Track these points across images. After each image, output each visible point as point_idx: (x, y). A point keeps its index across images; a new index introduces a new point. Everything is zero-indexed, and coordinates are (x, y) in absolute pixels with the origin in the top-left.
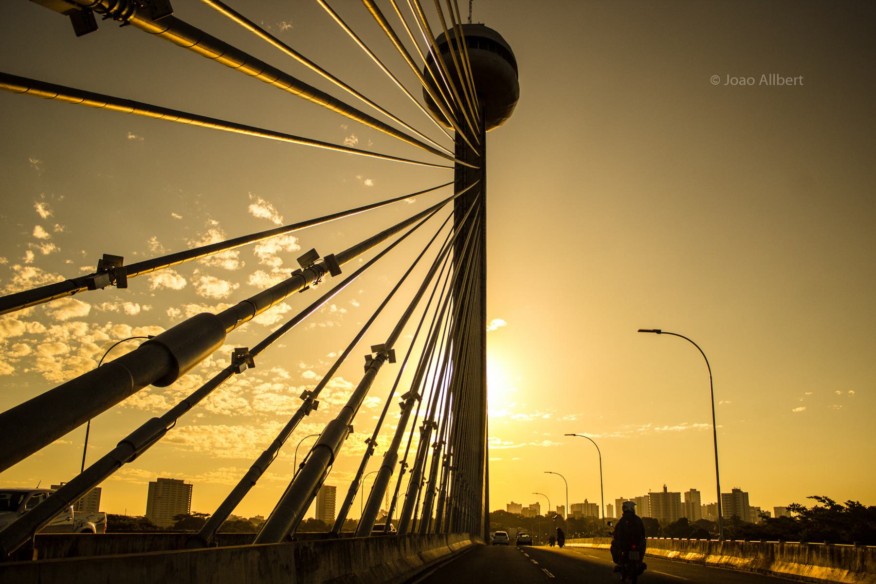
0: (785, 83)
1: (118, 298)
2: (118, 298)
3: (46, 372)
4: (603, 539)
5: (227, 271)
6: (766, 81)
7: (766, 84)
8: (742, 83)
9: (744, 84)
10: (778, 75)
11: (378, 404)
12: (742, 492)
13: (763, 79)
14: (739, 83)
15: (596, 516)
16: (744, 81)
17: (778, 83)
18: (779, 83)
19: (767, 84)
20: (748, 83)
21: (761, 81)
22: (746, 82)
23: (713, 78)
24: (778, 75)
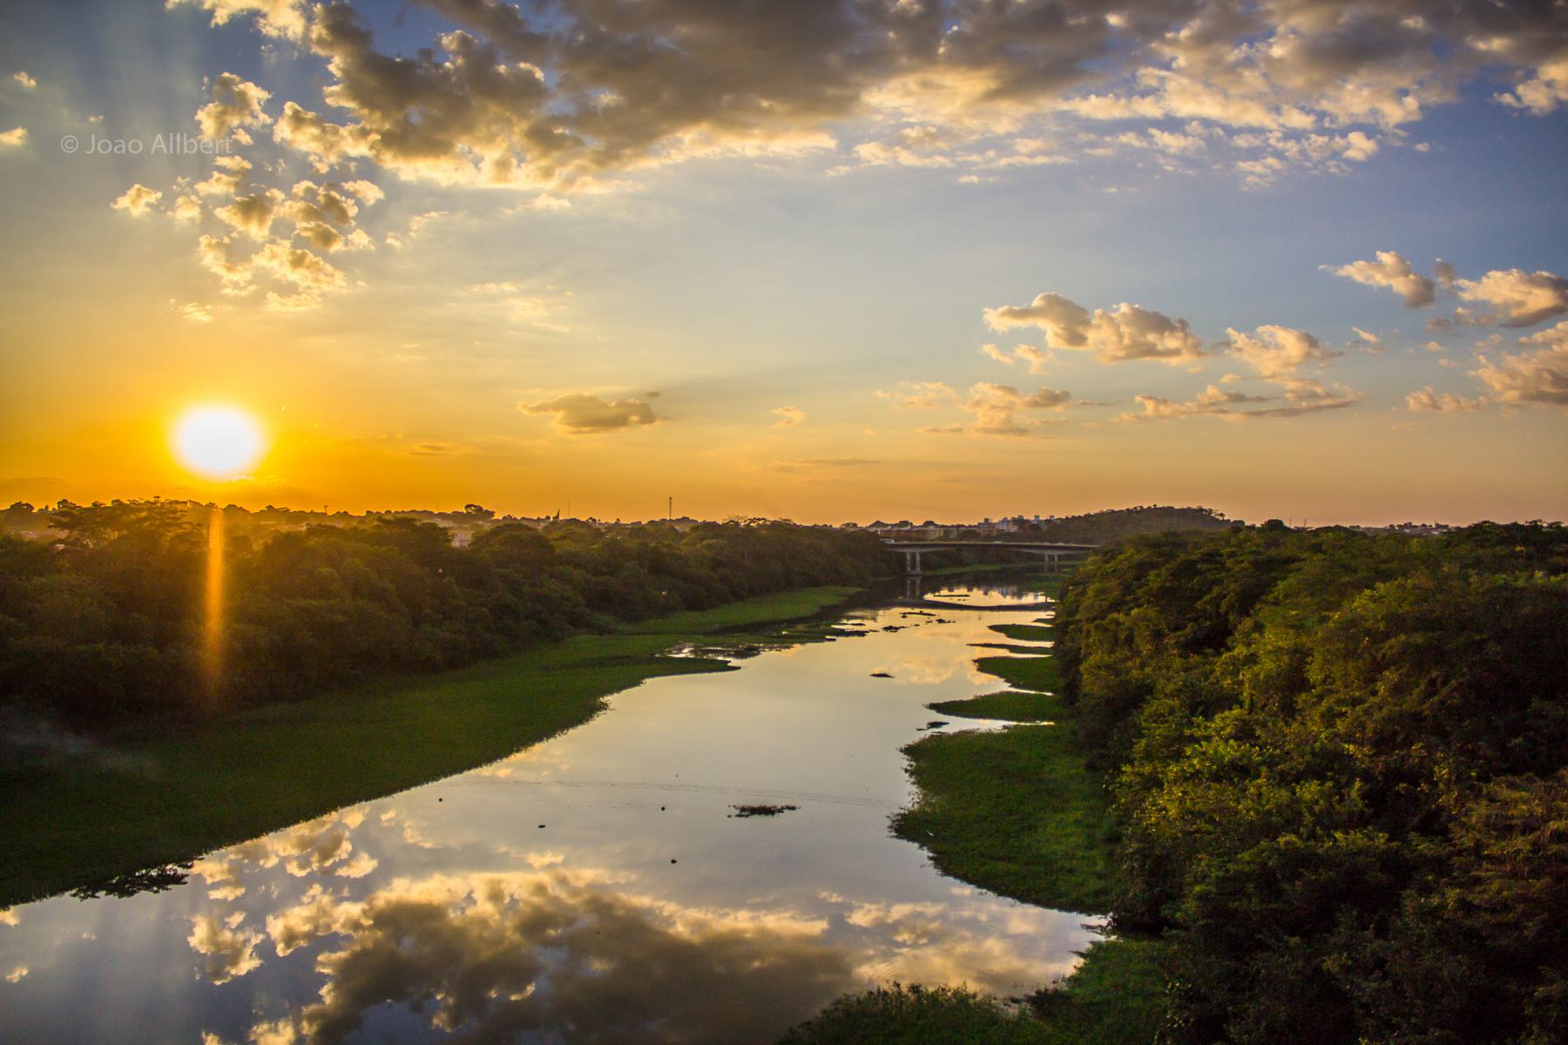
0: (199, 148)
1: (877, 531)
2: (877, 531)
3: (637, 423)
4: (634, 544)
5: (799, 623)
6: (163, 146)
7: (162, 151)
8: (120, 149)
9: (124, 151)
10: (185, 135)
11: (1304, 672)
12: (1252, 527)
13: (159, 143)
14: (113, 149)
15: (628, 531)
16: (124, 146)
17: (186, 151)
18: (188, 149)
19: (165, 151)
20: (131, 150)
21: (155, 146)
22: (127, 147)
23: (64, 141)
24: (185, 135)
